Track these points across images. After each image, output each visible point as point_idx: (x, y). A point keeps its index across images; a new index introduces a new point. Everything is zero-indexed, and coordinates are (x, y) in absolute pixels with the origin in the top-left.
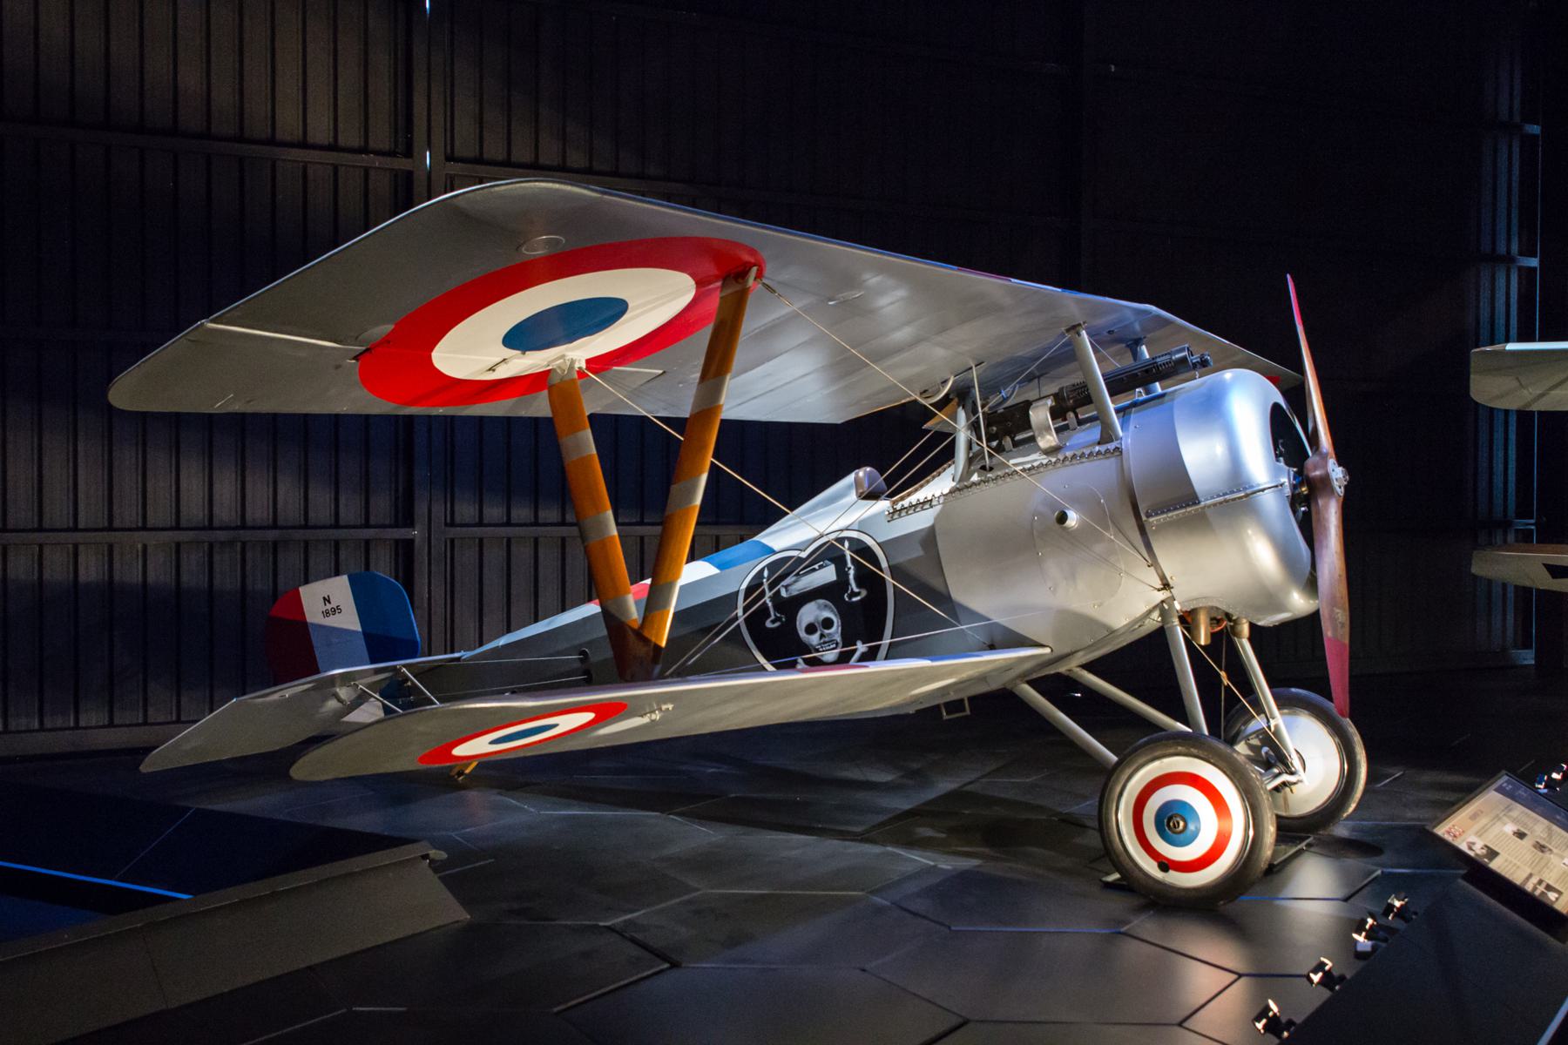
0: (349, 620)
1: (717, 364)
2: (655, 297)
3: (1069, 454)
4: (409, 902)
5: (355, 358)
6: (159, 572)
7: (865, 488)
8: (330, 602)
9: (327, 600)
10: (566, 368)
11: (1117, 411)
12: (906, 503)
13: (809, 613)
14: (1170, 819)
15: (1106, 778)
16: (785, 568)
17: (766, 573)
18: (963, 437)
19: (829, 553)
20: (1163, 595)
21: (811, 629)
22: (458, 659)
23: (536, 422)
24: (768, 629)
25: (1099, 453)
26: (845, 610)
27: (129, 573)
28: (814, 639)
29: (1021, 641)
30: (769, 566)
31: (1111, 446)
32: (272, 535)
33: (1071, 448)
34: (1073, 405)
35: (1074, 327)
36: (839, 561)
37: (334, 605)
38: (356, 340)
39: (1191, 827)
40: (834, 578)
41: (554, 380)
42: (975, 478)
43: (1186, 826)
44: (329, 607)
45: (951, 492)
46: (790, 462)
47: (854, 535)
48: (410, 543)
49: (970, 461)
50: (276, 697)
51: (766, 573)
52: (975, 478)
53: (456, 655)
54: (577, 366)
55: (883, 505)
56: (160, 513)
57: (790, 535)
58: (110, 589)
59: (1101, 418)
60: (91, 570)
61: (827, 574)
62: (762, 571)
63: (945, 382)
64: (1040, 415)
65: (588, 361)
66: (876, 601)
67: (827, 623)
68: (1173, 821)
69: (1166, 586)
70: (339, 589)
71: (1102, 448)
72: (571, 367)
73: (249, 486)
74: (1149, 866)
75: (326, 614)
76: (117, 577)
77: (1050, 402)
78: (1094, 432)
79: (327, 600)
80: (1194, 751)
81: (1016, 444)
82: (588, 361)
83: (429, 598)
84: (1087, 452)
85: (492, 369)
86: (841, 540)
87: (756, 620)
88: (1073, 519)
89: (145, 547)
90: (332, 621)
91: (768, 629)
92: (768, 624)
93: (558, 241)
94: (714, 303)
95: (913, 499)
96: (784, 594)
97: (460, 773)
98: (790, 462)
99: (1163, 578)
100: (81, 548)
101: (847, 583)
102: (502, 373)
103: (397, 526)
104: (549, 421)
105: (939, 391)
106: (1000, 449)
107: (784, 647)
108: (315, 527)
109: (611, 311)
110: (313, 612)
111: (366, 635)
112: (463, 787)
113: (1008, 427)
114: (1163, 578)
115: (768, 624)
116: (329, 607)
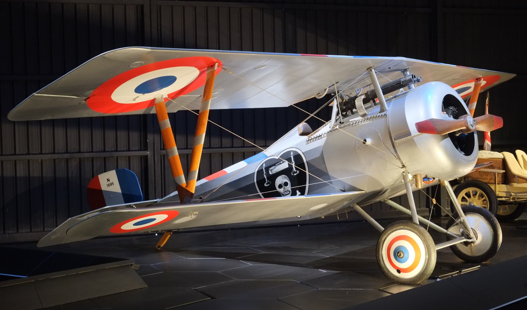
0: (117, 188)
1: (206, 94)
2: (185, 76)
3: (369, 117)
4: (123, 280)
5: (85, 100)
6: (48, 173)
7: (301, 131)
8: (109, 181)
9: (108, 180)
10: (160, 98)
11: (386, 101)
12: (313, 137)
13: (280, 180)
14: (398, 253)
15: (377, 236)
16: (274, 163)
17: (264, 165)
18: (335, 110)
19: (286, 156)
20: (403, 170)
21: (280, 186)
22: (156, 202)
23: (153, 114)
24: (264, 185)
25: (379, 116)
26: (291, 178)
27: (35, 172)
28: (281, 190)
29: (354, 189)
30: (265, 162)
31: (383, 113)
32: (66, 156)
33: (370, 115)
34: (371, 98)
35: (369, 68)
36: (289, 160)
37: (111, 182)
38: (83, 95)
39: (406, 255)
40: (287, 166)
41: (157, 102)
42: (337, 127)
43: (404, 255)
44: (109, 183)
45: (328, 132)
46: (271, 123)
47: (294, 149)
48: (146, 157)
49: (336, 120)
50: (85, 217)
51: (264, 165)
52: (337, 127)
53: (155, 200)
54: (164, 97)
55: (306, 138)
56: (47, 147)
57: (276, 150)
58: (29, 179)
59: (381, 104)
60: (21, 172)
61: (285, 165)
62: (263, 164)
63: (325, 90)
64: (359, 102)
65: (168, 95)
66: (301, 175)
67: (286, 184)
68: (398, 254)
69: (404, 166)
70: (112, 175)
71: (380, 114)
72: (162, 98)
73: (81, 133)
74: (394, 272)
75: (108, 185)
76: (31, 175)
77: (363, 97)
78: (377, 109)
79: (108, 180)
80: (406, 227)
81: (353, 113)
82: (168, 95)
83: (155, 180)
84: (375, 116)
85: (134, 100)
86: (290, 152)
87: (261, 182)
88: (369, 142)
89: (42, 161)
90: (111, 189)
91: (264, 185)
92: (265, 185)
93: (142, 63)
94: (205, 76)
95: (315, 135)
96: (270, 173)
97: (159, 247)
98: (271, 123)
99: (402, 163)
100: (17, 162)
101: (292, 168)
102: (138, 101)
103: (141, 150)
104: (156, 114)
105: (323, 94)
106: (345, 116)
107: (270, 192)
108: (108, 152)
109: (171, 80)
110: (104, 187)
111: (123, 194)
112: (158, 251)
113: (348, 107)
114: (402, 163)
115: (265, 185)
116: (109, 183)
